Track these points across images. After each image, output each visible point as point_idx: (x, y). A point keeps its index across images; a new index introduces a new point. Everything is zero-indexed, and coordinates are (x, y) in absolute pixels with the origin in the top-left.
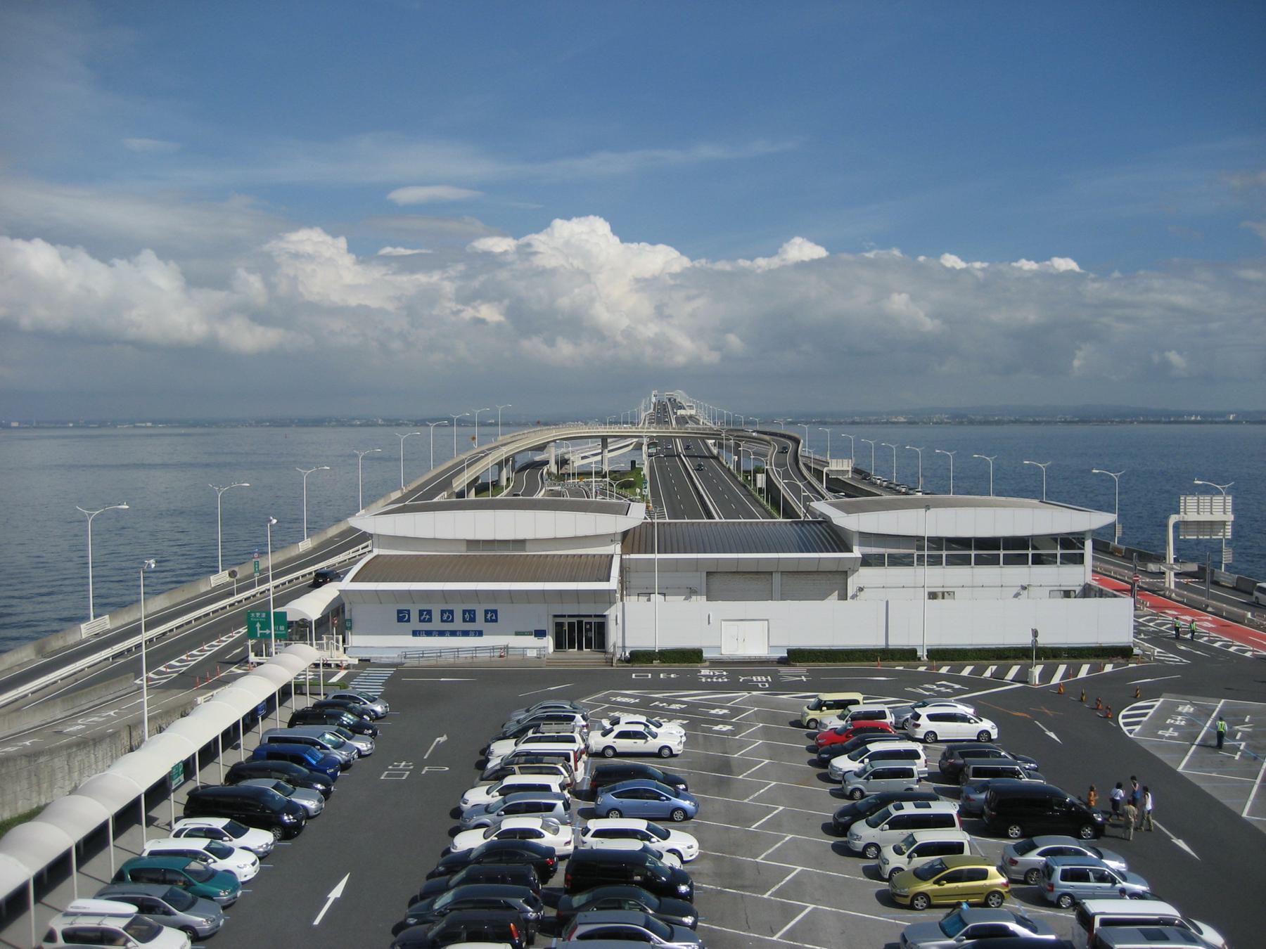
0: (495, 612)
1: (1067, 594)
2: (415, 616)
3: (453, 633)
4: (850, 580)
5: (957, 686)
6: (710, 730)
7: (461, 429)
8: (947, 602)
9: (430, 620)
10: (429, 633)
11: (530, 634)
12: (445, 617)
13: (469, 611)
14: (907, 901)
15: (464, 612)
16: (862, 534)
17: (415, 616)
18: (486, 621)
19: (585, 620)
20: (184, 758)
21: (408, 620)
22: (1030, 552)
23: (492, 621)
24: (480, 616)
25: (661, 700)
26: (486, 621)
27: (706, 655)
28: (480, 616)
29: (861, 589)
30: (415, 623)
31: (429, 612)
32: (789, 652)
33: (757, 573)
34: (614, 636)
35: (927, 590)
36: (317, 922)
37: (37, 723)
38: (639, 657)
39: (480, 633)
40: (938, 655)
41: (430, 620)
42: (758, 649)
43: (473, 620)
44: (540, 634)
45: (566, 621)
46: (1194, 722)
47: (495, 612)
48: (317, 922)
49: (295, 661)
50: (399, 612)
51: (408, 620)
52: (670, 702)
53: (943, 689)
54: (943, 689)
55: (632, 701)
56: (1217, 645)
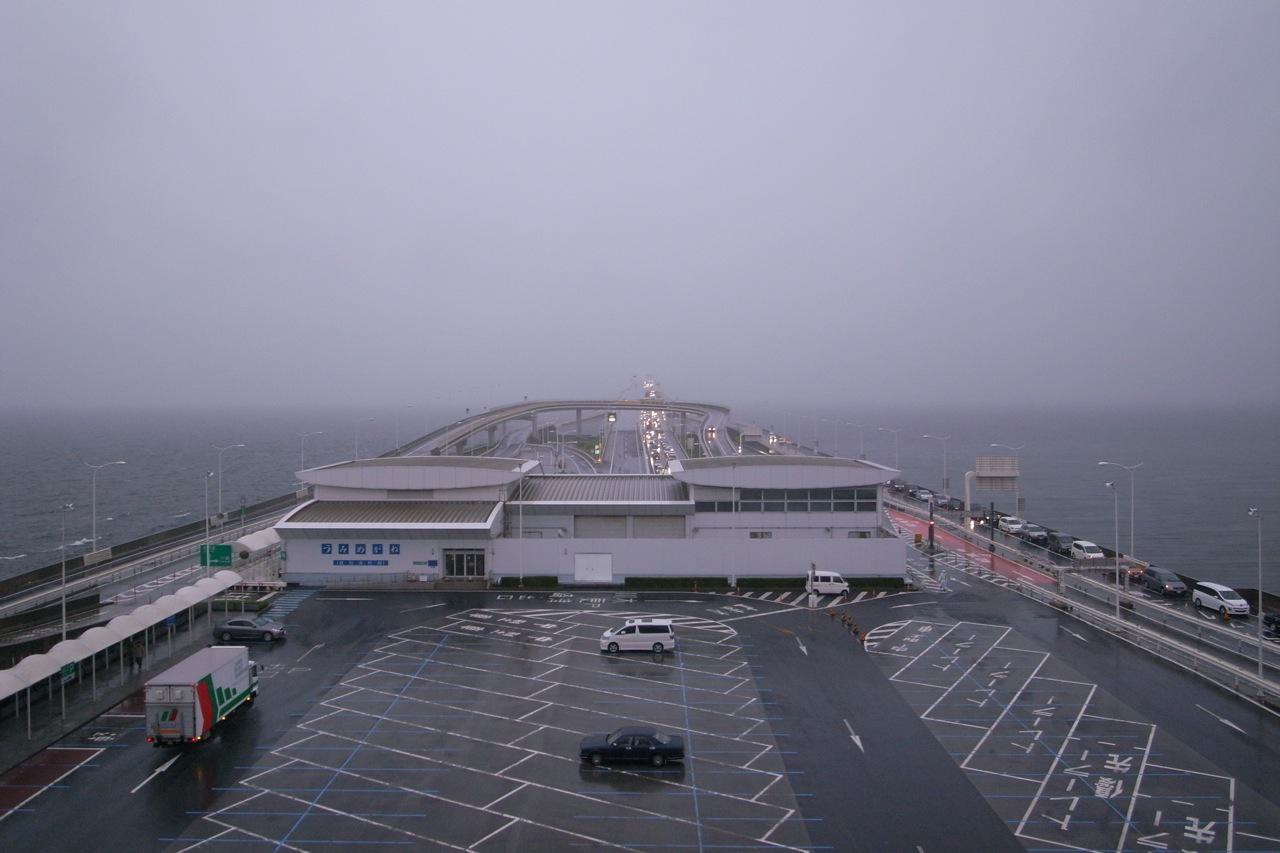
0: (398, 546)
1: (863, 535)
2: (335, 549)
3: (365, 563)
4: (687, 522)
5: (749, 608)
6: (533, 641)
7: (727, 499)
8: (765, 540)
9: (347, 552)
10: (346, 563)
11: (425, 563)
12: (359, 549)
13: (378, 545)
14: (586, 414)
15: (374, 546)
16: (695, 485)
17: (335, 549)
18: (391, 553)
19: (465, 553)
20: (85, 656)
21: (330, 553)
22: (832, 501)
23: (395, 553)
24: (386, 549)
25: (508, 617)
26: (391, 553)
27: (560, 581)
28: (386, 549)
29: (696, 530)
30: (336, 555)
31: (364, 546)
32: (627, 580)
33: (614, 516)
34: (488, 568)
35: (749, 531)
36: (133, 791)
37: (27, 630)
38: (509, 583)
39: (386, 563)
40: (745, 584)
41: (347, 552)
42: (604, 577)
43: (380, 552)
44: (433, 563)
45: (454, 554)
46: (926, 640)
47: (398, 546)
48: (133, 791)
49: (227, 578)
50: (323, 545)
51: (330, 553)
52: (514, 617)
53: (737, 610)
54: (737, 610)
55: (486, 617)
56: (1004, 585)
